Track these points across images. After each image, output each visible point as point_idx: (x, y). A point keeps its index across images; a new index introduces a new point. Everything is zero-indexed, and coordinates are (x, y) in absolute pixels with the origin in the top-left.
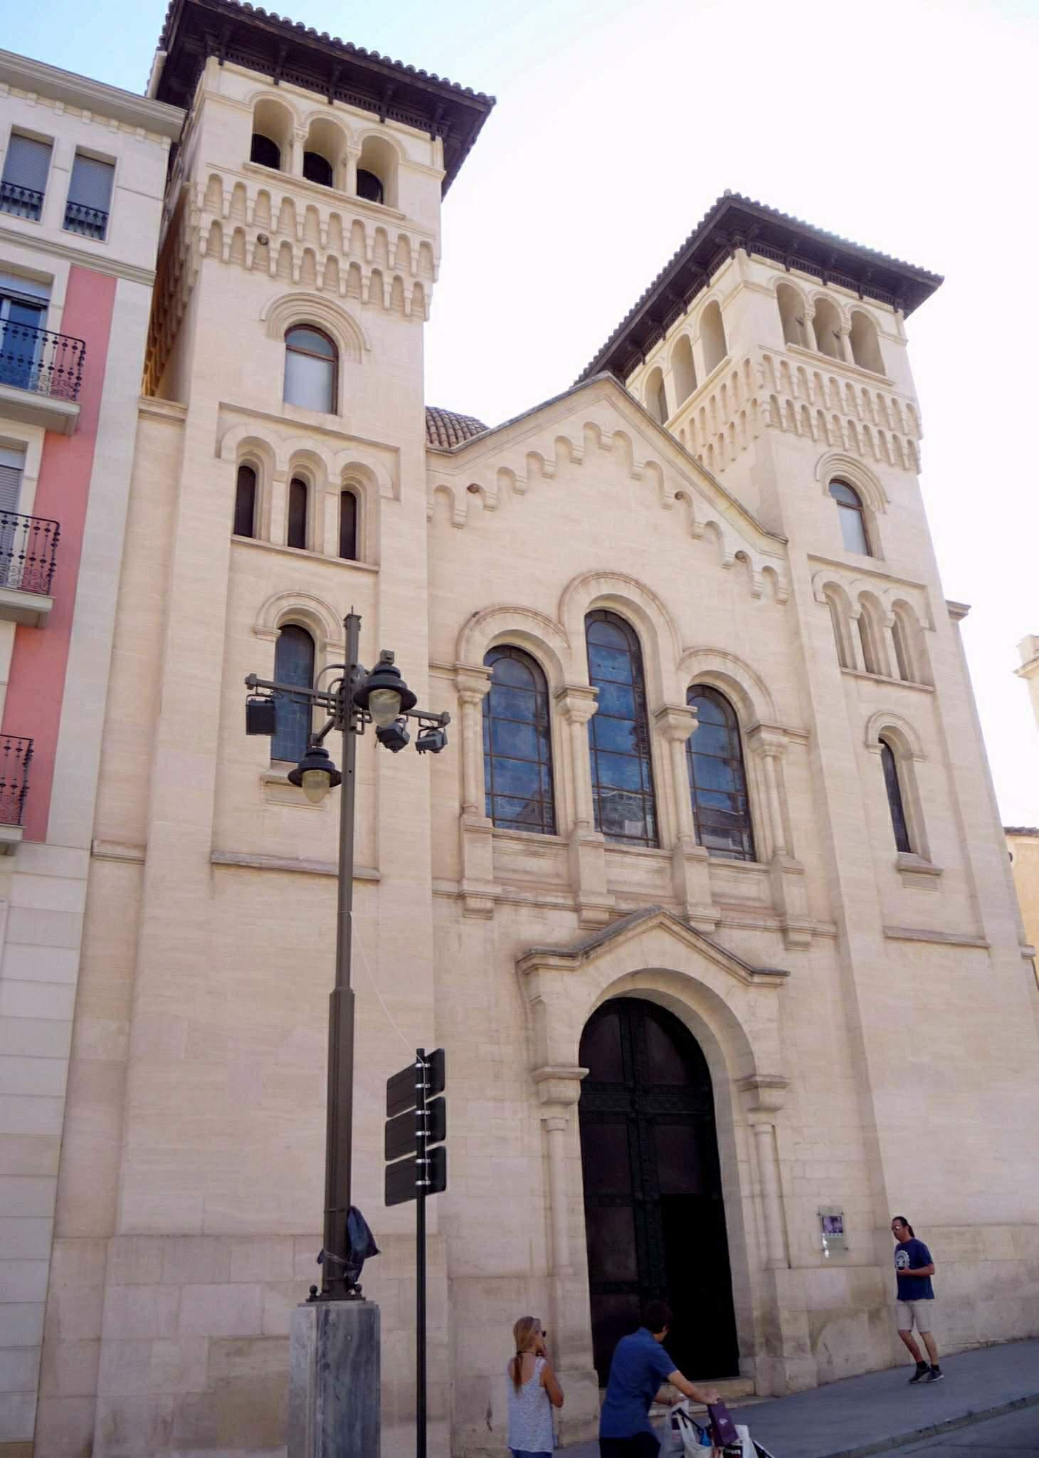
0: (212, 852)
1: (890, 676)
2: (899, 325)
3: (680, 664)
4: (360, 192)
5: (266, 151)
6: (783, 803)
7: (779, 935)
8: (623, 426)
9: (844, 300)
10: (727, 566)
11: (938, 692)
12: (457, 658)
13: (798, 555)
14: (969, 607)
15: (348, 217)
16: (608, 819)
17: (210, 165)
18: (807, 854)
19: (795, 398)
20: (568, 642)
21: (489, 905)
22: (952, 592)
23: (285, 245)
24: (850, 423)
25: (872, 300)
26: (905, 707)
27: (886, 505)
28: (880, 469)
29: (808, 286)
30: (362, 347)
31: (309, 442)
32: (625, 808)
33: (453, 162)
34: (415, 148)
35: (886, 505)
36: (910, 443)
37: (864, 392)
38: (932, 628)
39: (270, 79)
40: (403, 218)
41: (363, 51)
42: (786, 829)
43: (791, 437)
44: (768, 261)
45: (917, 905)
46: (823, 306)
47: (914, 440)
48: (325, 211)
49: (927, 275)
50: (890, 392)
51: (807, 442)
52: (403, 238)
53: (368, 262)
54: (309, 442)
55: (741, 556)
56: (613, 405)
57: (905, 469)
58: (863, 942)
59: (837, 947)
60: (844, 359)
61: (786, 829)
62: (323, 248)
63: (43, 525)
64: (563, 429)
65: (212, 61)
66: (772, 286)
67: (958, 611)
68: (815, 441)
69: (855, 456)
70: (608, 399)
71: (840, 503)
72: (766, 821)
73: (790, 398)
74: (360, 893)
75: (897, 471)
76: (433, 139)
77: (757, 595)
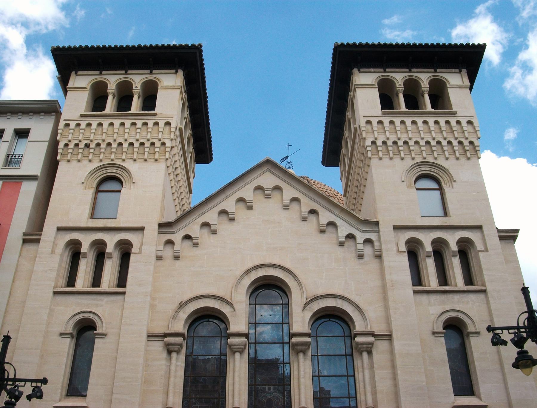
3: (304, 307)
4: (407, 106)
5: (387, 102)
6: (373, 377)
8: (278, 182)
10: (341, 244)
12: (492, 320)
13: (386, 229)
14: (517, 231)
17: (364, 117)
19: (399, 139)
20: (233, 308)
22: (502, 224)
30: (452, 180)
31: (99, 236)
33: (472, 78)
34: (454, 79)
35: (453, 183)
40: (455, 113)
42: (374, 393)
43: (386, 161)
51: (397, 161)
54: (99, 236)
55: (350, 237)
56: (273, 173)
61: (374, 393)
65: (355, 71)
67: (509, 236)
68: (402, 159)
69: (430, 160)
70: (269, 170)
72: (362, 390)
77: (361, 257)
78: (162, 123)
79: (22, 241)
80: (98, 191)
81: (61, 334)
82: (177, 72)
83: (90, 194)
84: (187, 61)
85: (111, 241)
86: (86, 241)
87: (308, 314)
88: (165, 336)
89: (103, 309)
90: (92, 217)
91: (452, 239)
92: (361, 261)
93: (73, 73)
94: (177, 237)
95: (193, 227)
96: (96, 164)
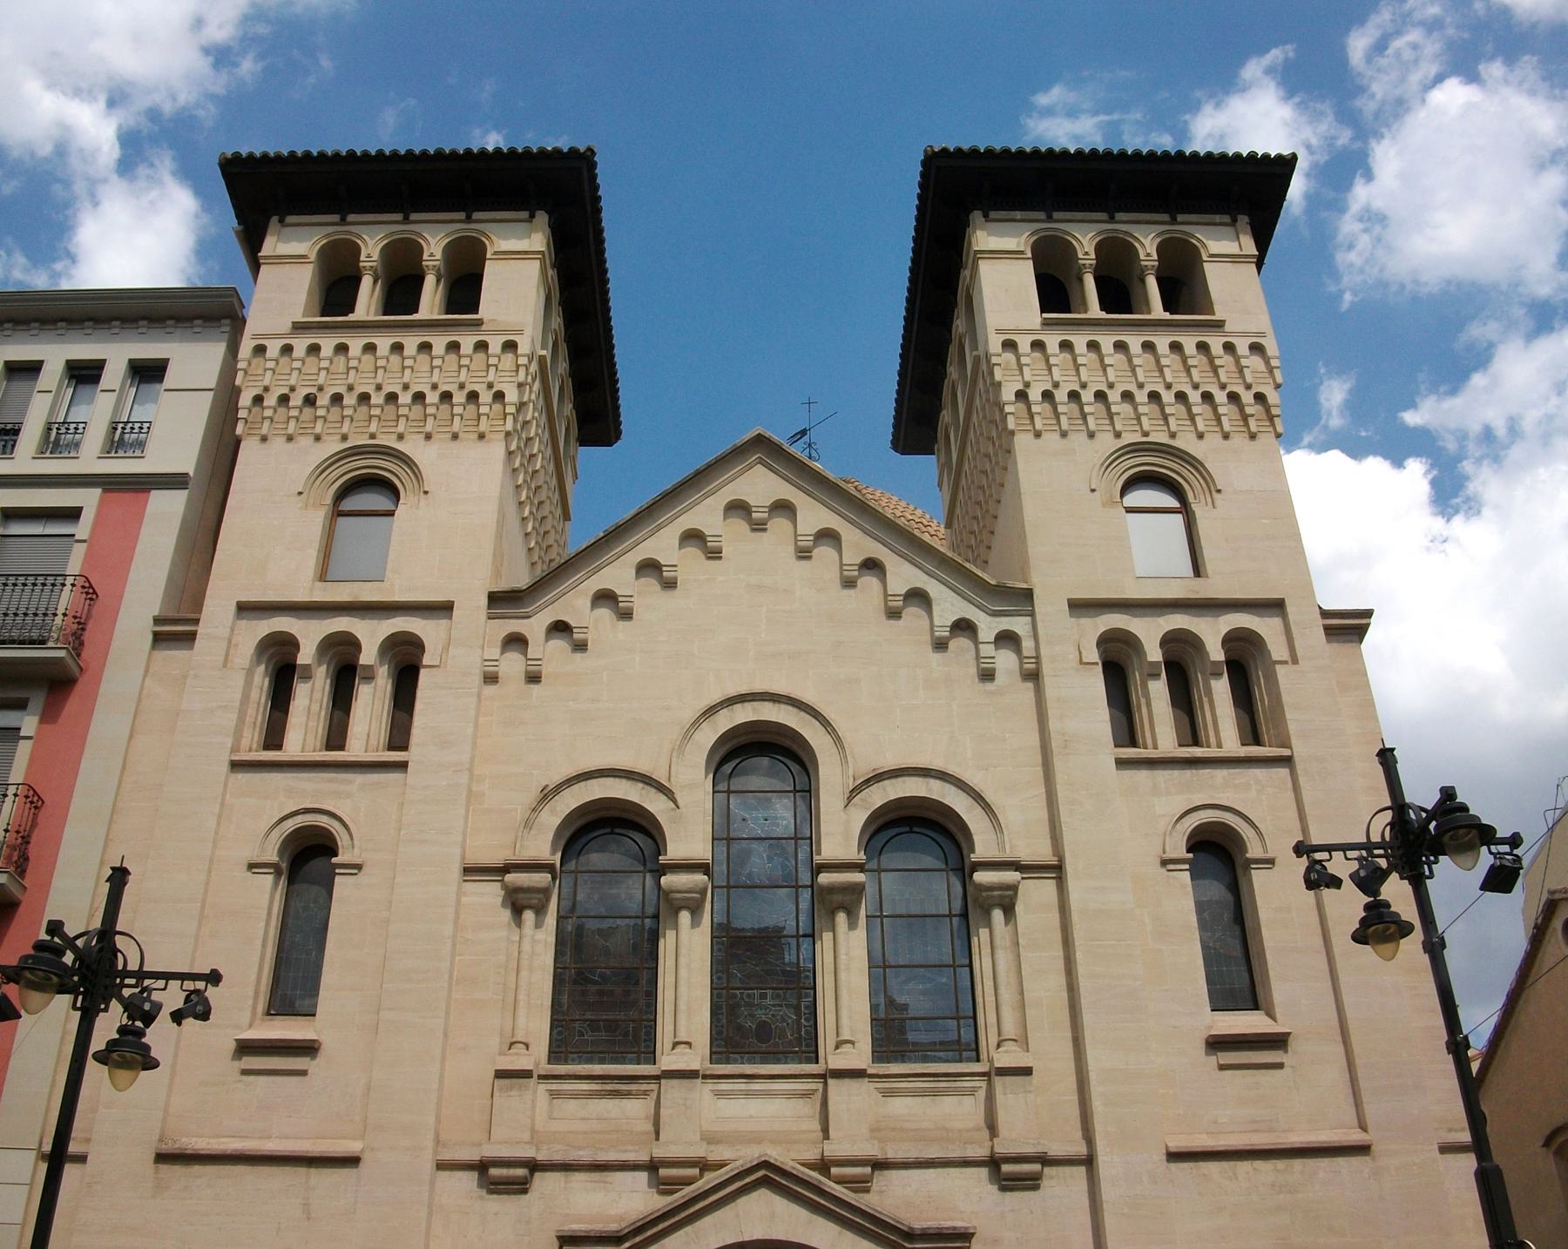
0: (160, 1140)
7: (537, 1175)
11: (1297, 759)
13: (1050, 606)
14: (1368, 614)
15: (1162, 342)
16: (893, 1036)
17: (999, 331)
18: (1049, 1051)
21: (521, 1172)
23: (1127, 396)
25: (1068, 215)
27: (1216, 495)
31: (1178, 621)
32: (764, 1014)
39: (399, 217)
41: (424, 153)
44: (1018, 215)
45: (1234, 1105)
48: (1189, 342)
51: (1078, 439)
52: (1229, 348)
53: (435, 387)
54: (1178, 621)
62: (1111, 386)
64: (688, 521)
67: (1349, 627)
69: (1161, 437)
70: (761, 462)
74: (70, 1172)
76: (1234, 221)
78: (495, 344)
79: (150, 637)
80: (337, 513)
81: (251, 866)
82: (532, 216)
83: (317, 518)
84: (556, 189)
85: (371, 635)
86: (309, 635)
87: (859, 817)
88: (507, 869)
89: (351, 804)
90: (323, 575)
91: (371, 635)
92: (989, 686)
93: (275, 219)
94: (535, 626)
95: (573, 603)
96: (333, 446)
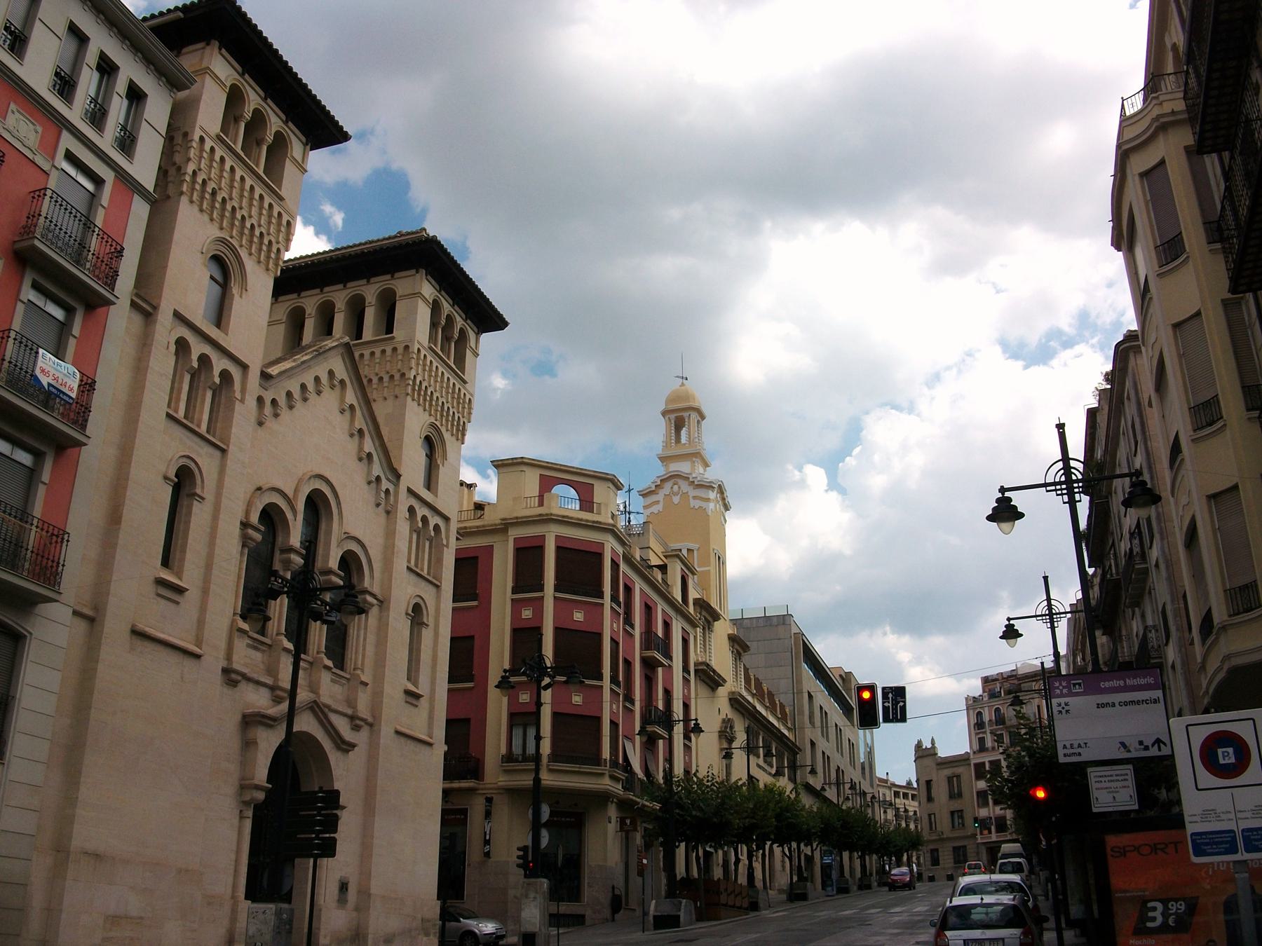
1: (199, 426)
2: (304, 156)
9: (275, 122)
24: (270, 242)
26: (206, 460)
28: (447, 436)
29: (254, 99)
36: (278, 250)
37: (242, 178)
38: (242, 401)
46: (450, 319)
47: (282, 249)
49: (500, 317)
50: (280, 205)
57: (201, 210)
58: (386, 731)
59: (372, 732)
60: (257, 165)
63: (24, 340)
66: (228, 85)
71: (212, 277)
73: (237, 206)
75: (454, 439)
